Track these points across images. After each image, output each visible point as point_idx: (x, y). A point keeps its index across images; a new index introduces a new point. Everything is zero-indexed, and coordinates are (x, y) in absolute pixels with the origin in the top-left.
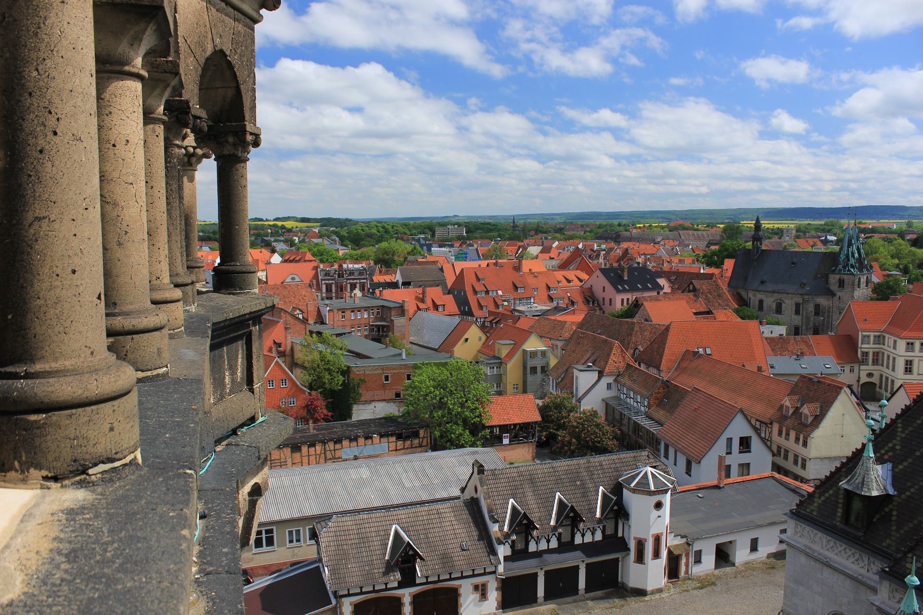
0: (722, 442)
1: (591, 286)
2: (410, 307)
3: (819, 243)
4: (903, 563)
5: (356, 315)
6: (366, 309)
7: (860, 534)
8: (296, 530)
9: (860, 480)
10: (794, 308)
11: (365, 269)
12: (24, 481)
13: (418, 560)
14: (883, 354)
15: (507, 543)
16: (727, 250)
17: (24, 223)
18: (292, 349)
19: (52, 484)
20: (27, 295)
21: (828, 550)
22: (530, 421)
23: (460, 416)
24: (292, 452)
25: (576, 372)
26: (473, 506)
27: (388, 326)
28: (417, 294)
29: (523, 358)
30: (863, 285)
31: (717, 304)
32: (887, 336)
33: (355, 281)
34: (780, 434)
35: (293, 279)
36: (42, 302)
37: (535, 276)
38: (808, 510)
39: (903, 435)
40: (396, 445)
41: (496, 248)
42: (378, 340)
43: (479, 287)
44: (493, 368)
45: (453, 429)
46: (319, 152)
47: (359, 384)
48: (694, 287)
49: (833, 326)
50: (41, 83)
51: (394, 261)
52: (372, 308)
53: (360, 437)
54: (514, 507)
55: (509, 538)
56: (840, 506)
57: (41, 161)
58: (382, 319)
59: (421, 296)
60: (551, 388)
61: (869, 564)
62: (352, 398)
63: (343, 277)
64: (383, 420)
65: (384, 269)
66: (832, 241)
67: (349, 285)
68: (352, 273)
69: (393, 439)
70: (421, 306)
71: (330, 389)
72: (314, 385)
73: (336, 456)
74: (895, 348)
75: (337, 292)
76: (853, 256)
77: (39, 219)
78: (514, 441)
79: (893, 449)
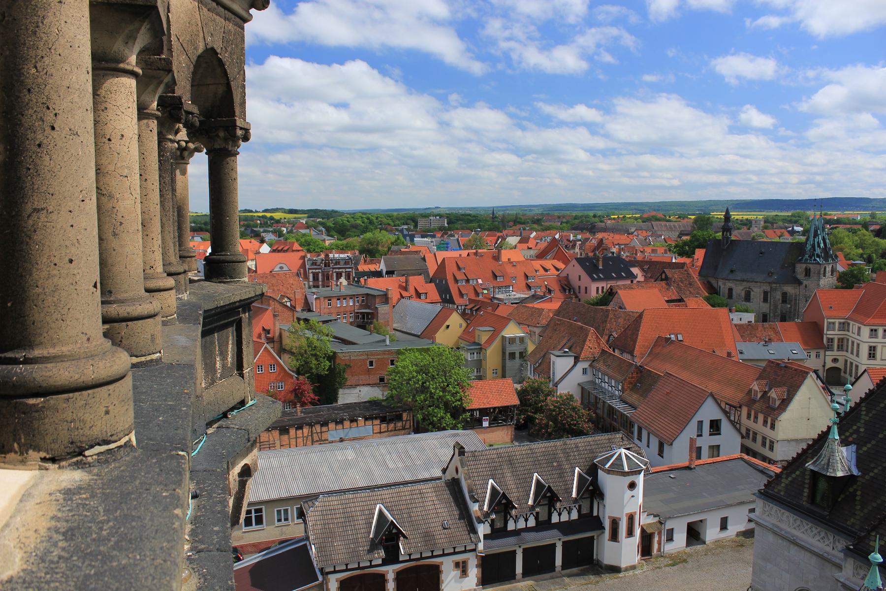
0: (693, 425)
1: (568, 274)
2: (394, 295)
3: (786, 233)
4: (867, 541)
5: (341, 303)
6: (352, 297)
7: (826, 513)
8: (284, 510)
9: (825, 461)
10: (762, 296)
11: (350, 259)
12: (23, 462)
13: (402, 538)
14: (848, 340)
15: (487, 522)
16: (697, 240)
17: (23, 215)
18: (280, 336)
19: (50, 465)
20: (26, 283)
21: (795, 528)
22: (509, 404)
23: (442, 399)
24: (281, 434)
25: (553, 358)
26: (454, 486)
27: (372, 313)
28: (400, 283)
29: (502, 344)
30: (828, 274)
31: (688, 292)
32: (851, 323)
33: (341, 270)
34: (749, 417)
35: (281, 268)
36: (40, 290)
37: (514, 266)
38: (776, 490)
39: (867, 418)
40: (380, 428)
41: (476, 239)
42: (362, 326)
43: (459, 276)
44: (473, 353)
45: (435, 413)
46: (306, 146)
47: (345, 369)
48: (666, 276)
49: (800, 314)
50: (40, 80)
51: (378, 251)
52: (357, 296)
53: (345, 420)
54: (493, 488)
55: (489, 517)
56: (807, 486)
57: (39, 155)
58: (367, 306)
59: (404, 284)
60: (529, 373)
61: (834, 542)
62: (338, 383)
63: (329, 266)
64: (368, 404)
65: (368, 259)
66: (798, 232)
67: (335, 274)
68: (337, 262)
69: (377, 422)
70: (404, 294)
71: (317, 374)
72: (302, 370)
73: (323, 439)
74: (859, 334)
75: (323, 281)
76: (819, 246)
77: (37, 210)
78: (493, 424)
79: (857, 431)
